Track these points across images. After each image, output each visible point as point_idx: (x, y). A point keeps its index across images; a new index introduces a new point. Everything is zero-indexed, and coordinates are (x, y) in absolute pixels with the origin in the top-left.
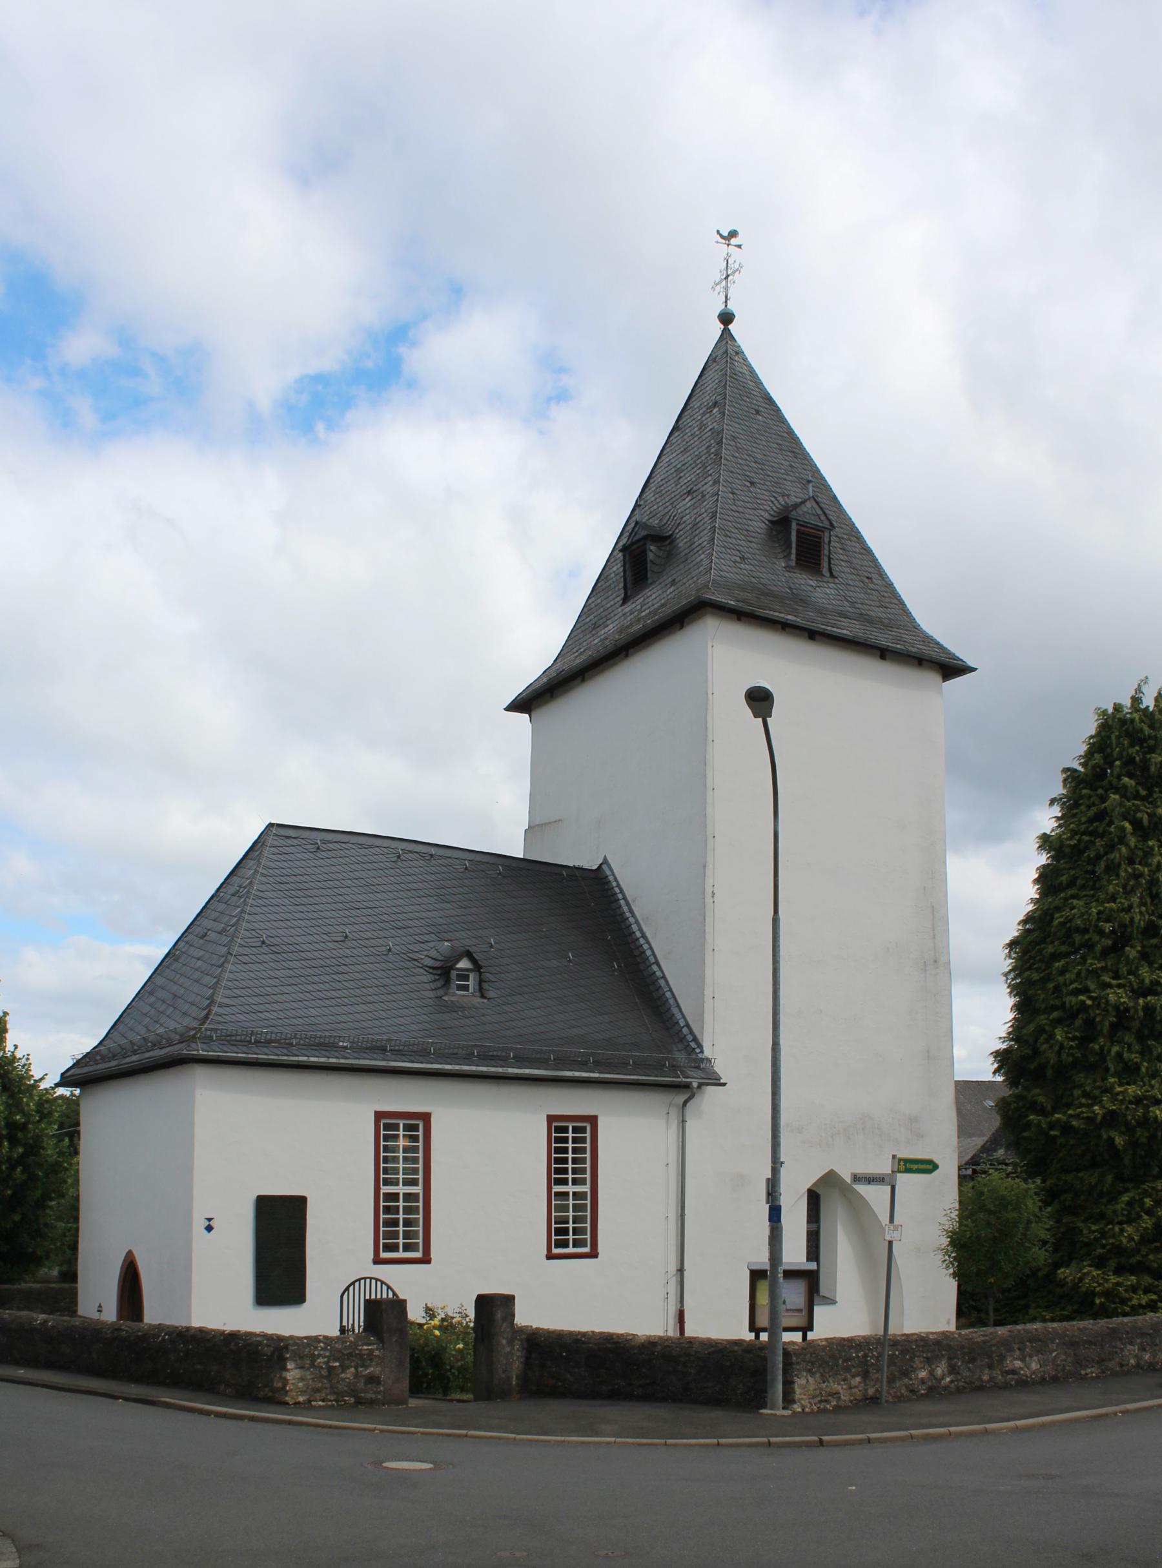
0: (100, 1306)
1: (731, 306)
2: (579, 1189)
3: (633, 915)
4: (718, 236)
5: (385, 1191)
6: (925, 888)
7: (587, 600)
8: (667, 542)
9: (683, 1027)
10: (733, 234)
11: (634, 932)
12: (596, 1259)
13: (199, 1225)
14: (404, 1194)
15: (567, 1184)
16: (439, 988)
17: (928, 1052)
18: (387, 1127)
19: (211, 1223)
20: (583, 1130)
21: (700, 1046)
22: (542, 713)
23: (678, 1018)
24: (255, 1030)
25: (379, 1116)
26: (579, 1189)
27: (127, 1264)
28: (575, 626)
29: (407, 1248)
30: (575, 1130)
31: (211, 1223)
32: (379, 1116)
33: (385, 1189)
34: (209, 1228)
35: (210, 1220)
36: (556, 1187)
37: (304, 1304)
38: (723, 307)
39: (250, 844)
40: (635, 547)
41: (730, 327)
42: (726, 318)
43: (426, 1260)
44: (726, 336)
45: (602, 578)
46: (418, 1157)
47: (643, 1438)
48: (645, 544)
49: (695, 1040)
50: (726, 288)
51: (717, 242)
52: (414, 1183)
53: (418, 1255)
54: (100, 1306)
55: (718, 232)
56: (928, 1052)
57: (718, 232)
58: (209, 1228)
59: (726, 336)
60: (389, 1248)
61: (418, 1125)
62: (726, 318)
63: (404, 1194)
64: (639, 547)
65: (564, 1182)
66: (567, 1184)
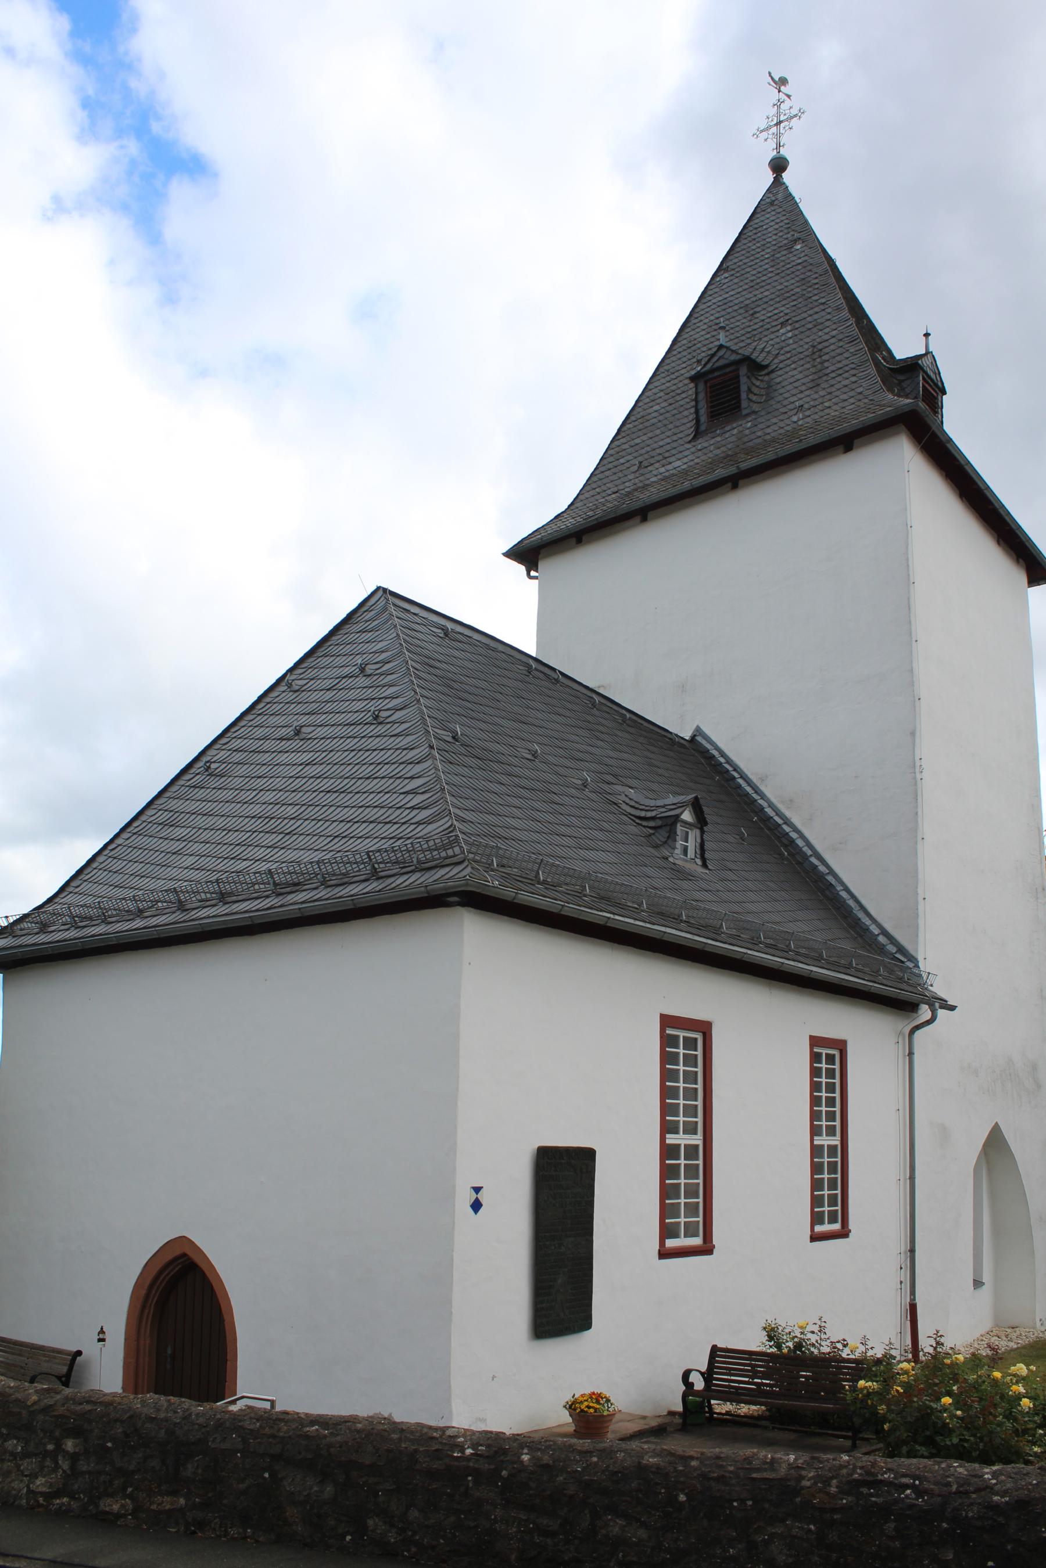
0: (102, 1331)
3: (763, 796)
4: (770, 78)
6: (1033, 806)
7: (612, 442)
8: (763, 373)
9: (878, 935)
11: (772, 817)
13: (466, 1198)
17: (1041, 990)
21: (914, 960)
22: (551, 566)
23: (867, 923)
24: (546, 859)
27: (169, 1257)
28: (595, 469)
34: (476, 1206)
35: (477, 1190)
37: (587, 1334)
38: (775, 153)
39: (344, 616)
40: (717, 374)
42: (779, 166)
44: (778, 182)
45: (633, 418)
46: (834, 1083)
47: (232, 1397)
48: (738, 369)
49: (901, 949)
50: (778, 136)
51: (770, 85)
54: (102, 1331)
55: (770, 73)
56: (1041, 990)
57: (770, 73)
58: (476, 1206)
59: (778, 182)
62: (779, 166)
64: (730, 372)
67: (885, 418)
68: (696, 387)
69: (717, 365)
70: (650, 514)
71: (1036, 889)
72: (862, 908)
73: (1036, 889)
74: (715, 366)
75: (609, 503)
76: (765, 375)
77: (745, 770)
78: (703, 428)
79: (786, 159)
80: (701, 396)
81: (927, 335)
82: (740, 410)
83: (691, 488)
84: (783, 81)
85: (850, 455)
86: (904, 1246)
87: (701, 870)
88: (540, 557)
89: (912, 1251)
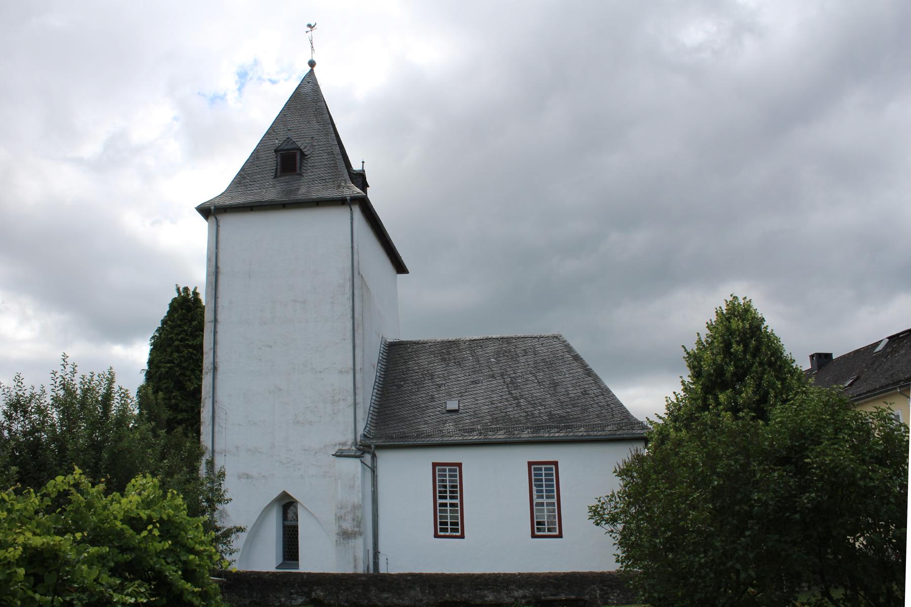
2: (454, 501)
5: (440, 502)
10: (309, 26)
12: (463, 540)
14: (450, 503)
15: (447, 499)
16: (377, 401)
18: (535, 469)
20: (455, 471)
25: (530, 464)
26: (454, 501)
29: (549, 530)
30: (546, 469)
32: (530, 464)
36: (457, 502)
42: (312, 64)
43: (462, 536)
44: (312, 72)
52: (455, 498)
53: (459, 534)
59: (312, 72)
60: (539, 530)
61: (456, 469)
62: (312, 64)
63: (450, 503)
65: (445, 498)
66: (447, 499)
81: (363, 162)
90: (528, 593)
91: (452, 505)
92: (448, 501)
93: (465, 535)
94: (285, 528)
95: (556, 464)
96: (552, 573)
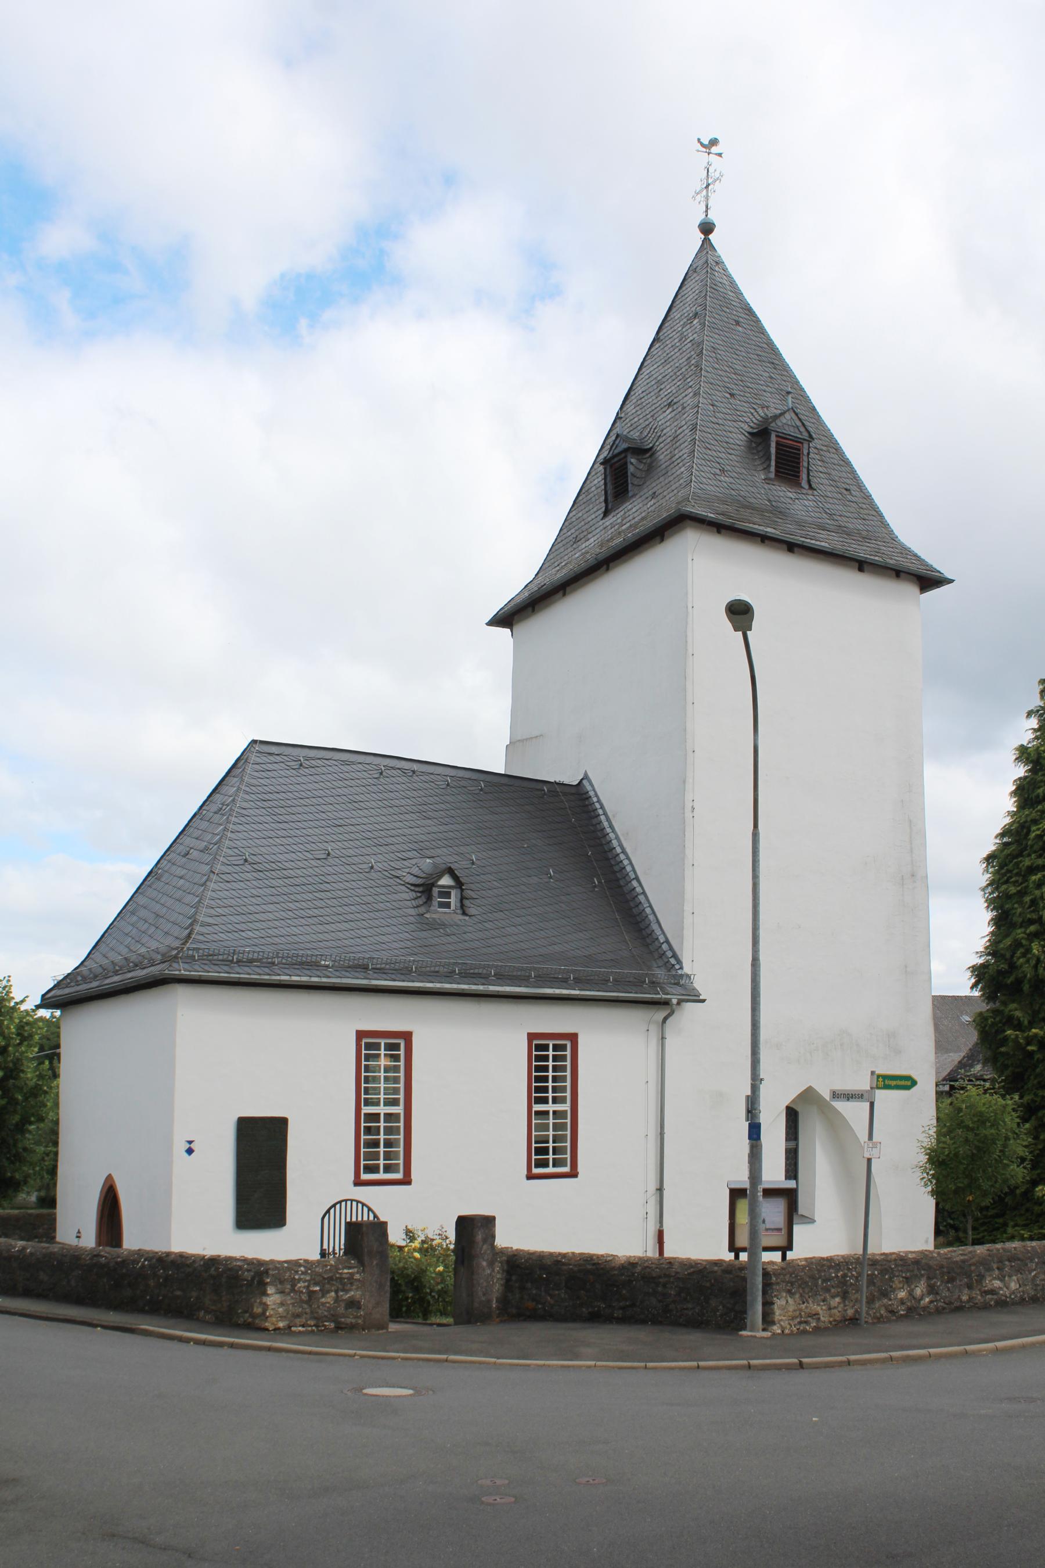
1: (712, 216)
2: (559, 1107)
8: (648, 455)
13: (181, 1147)
14: (385, 1114)
17: (906, 967)
19: (192, 1146)
20: (563, 1048)
22: (521, 628)
24: (237, 949)
25: (360, 1035)
26: (559, 1107)
30: (556, 1048)
31: (192, 1146)
32: (360, 1035)
33: (366, 1110)
35: (190, 1142)
37: (284, 1227)
40: (616, 460)
41: (711, 237)
42: (707, 228)
43: (573, 1174)
44: (707, 245)
45: (583, 491)
49: (675, 956)
50: (707, 198)
51: (698, 151)
53: (566, 1169)
56: (906, 967)
57: (699, 140)
58: (190, 1151)
59: (707, 245)
62: (707, 228)
65: (545, 1101)
67: (664, 522)
68: (605, 469)
69: (616, 451)
70: (568, 589)
71: (903, 876)
72: (658, 922)
73: (903, 876)
74: (614, 453)
75: (576, 559)
76: (648, 458)
77: (608, 811)
78: (610, 507)
79: (714, 224)
80: (608, 478)
82: (628, 492)
83: (596, 562)
84: (714, 142)
85: (663, 545)
86: (652, 1186)
87: (459, 917)
88: (514, 623)
89: (660, 1190)
90: (961, 1281)
91: (389, 1117)
92: (550, 1107)
93: (413, 1177)
94: (759, 1138)
95: (407, 1036)
96: (584, 1254)
